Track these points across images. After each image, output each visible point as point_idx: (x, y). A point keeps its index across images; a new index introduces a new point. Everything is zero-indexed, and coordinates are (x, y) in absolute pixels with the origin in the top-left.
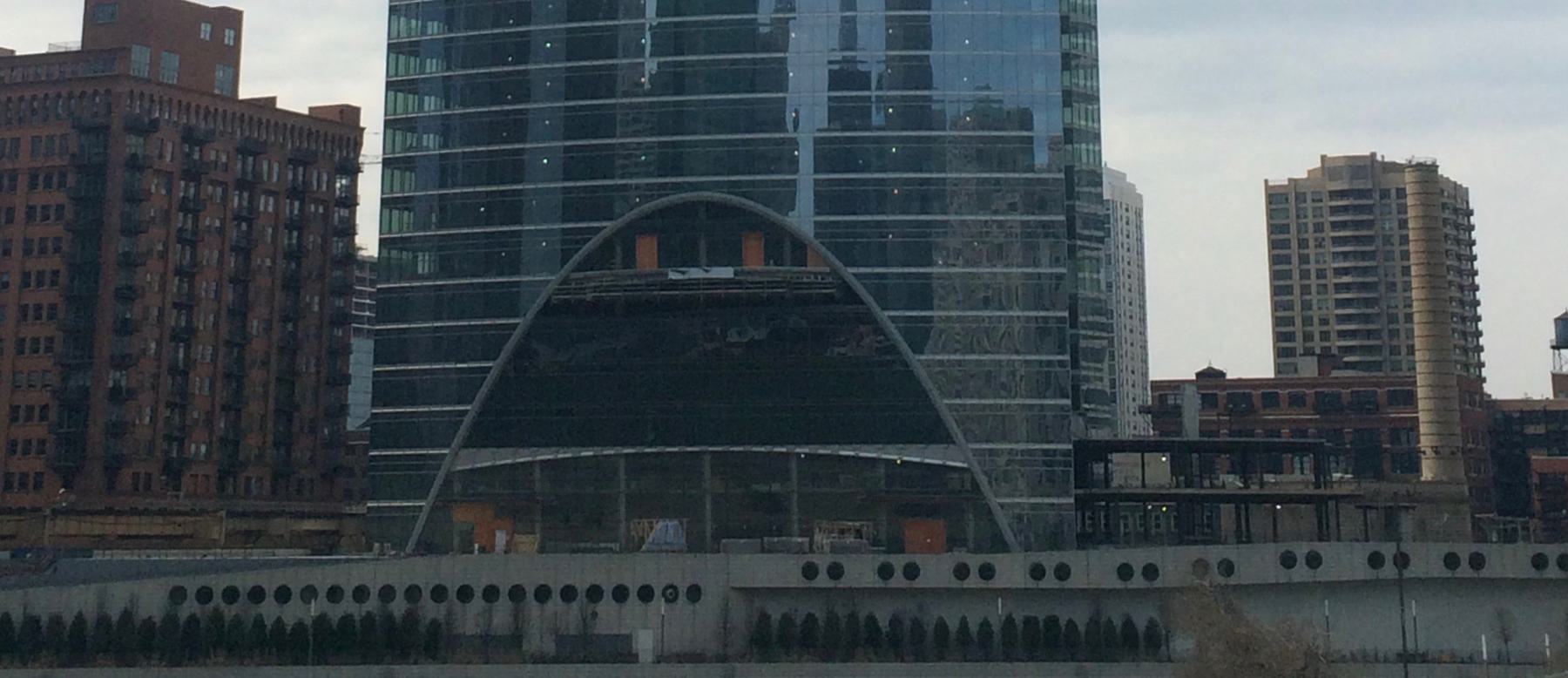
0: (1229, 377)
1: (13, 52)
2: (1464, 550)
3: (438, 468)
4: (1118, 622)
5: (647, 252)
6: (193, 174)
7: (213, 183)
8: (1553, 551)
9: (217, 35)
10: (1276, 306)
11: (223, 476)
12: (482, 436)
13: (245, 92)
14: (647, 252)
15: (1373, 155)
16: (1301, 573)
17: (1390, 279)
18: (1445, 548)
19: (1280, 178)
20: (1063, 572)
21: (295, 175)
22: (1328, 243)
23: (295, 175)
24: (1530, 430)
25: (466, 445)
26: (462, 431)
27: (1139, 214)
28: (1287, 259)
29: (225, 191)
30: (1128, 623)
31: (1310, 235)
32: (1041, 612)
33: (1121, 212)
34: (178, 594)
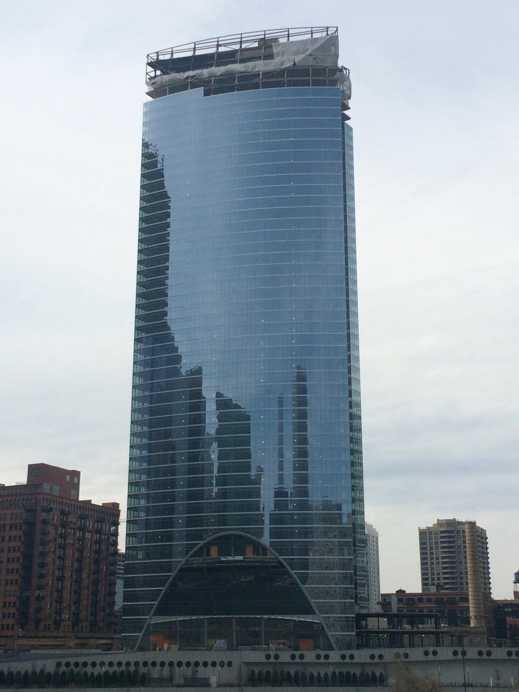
0: (407, 592)
1: (4, 485)
2: (485, 650)
3: (145, 622)
4: (370, 674)
5: (214, 551)
6: (64, 525)
7: (71, 528)
8: (514, 650)
9: (72, 479)
10: (422, 569)
11: (74, 625)
12: (159, 612)
13: (81, 498)
14: (214, 551)
15: (455, 519)
16: (431, 657)
17: (460, 560)
18: (479, 649)
19: (424, 527)
20: (352, 657)
21: (98, 526)
22: (440, 548)
23: (98, 526)
24: (507, 610)
25: (154, 615)
26: (153, 610)
27: (377, 538)
28: (427, 574)
29: (74, 531)
30: (374, 674)
31: (434, 546)
32: (344, 670)
33: (371, 538)
34: (59, 664)
